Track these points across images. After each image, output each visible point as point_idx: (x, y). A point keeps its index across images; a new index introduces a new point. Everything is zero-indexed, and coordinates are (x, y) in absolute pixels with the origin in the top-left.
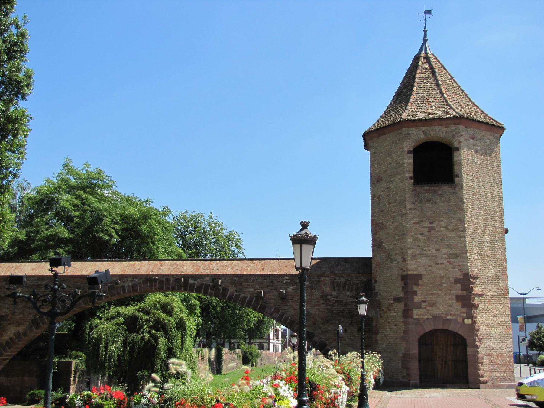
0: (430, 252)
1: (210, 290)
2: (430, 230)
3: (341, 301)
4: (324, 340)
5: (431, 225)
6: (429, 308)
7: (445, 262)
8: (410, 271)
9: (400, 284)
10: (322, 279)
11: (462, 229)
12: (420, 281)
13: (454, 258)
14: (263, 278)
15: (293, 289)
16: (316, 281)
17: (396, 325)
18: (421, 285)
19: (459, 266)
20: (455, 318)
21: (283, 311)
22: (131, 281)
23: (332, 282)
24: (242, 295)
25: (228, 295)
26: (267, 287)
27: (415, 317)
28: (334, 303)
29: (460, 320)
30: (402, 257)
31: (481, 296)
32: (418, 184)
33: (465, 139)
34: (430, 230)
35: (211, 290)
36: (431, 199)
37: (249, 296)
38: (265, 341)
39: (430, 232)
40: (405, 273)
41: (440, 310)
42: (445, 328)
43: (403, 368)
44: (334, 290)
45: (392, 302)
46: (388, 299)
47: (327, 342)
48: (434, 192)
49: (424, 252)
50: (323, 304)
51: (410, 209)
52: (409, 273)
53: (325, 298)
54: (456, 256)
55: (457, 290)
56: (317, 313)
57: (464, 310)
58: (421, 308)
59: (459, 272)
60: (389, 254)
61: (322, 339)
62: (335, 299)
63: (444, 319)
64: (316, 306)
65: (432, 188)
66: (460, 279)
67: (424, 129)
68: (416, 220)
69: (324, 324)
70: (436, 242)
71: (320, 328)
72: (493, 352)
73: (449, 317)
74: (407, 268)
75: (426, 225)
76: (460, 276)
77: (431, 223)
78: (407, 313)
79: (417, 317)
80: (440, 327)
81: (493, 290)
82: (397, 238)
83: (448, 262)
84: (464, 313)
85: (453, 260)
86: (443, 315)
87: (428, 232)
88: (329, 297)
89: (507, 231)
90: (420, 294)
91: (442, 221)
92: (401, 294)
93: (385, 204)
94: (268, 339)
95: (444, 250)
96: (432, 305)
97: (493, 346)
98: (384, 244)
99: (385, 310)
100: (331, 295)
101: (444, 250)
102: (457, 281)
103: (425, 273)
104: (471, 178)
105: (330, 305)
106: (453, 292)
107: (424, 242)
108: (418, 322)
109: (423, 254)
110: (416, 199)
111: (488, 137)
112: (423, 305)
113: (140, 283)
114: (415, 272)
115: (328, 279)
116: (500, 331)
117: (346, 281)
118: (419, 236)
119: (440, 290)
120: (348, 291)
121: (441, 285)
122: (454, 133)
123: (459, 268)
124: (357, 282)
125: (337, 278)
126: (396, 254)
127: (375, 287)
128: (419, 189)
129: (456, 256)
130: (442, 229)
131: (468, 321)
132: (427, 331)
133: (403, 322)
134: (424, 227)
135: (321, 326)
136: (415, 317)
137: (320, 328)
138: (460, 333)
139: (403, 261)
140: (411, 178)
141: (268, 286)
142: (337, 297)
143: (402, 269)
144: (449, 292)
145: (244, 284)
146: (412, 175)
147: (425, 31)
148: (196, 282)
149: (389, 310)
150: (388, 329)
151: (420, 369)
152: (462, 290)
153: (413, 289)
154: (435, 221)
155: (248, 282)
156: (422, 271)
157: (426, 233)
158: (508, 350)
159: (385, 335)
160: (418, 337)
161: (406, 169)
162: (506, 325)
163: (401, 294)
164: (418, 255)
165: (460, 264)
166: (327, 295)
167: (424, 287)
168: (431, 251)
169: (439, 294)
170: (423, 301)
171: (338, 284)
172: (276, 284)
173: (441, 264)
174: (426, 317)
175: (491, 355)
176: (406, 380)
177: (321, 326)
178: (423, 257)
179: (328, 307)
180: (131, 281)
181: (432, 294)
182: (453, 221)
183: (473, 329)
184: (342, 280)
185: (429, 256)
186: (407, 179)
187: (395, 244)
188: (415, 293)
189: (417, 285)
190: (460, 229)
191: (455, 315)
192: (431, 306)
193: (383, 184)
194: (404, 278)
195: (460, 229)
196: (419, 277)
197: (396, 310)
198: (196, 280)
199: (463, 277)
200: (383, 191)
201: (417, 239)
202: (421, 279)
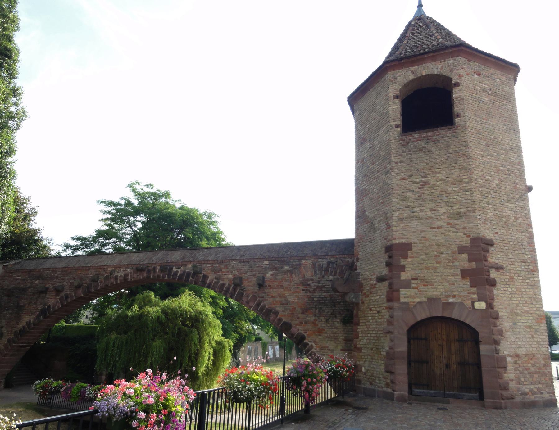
0: (423, 213)
1: (191, 278)
2: (423, 185)
3: (324, 287)
4: (302, 332)
5: (423, 179)
6: (422, 288)
8: (395, 239)
9: (384, 258)
10: (303, 262)
11: (467, 180)
12: (409, 251)
13: (457, 218)
14: (242, 263)
15: (272, 275)
16: (297, 265)
17: (378, 312)
18: (411, 257)
19: (464, 228)
20: (459, 300)
21: (261, 299)
22: (124, 271)
23: (314, 265)
24: (221, 282)
25: (208, 283)
26: (246, 273)
27: (402, 300)
28: (315, 289)
29: (468, 304)
30: (387, 224)
31: (499, 268)
32: (406, 132)
33: (468, 74)
34: (423, 185)
35: (192, 278)
36: (424, 147)
37: (227, 283)
39: (423, 188)
40: (389, 243)
41: (439, 290)
42: (446, 315)
43: (387, 372)
45: (375, 282)
46: (371, 279)
47: (305, 335)
48: (428, 138)
49: (415, 214)
50: (303, 290)
51: (396, 163)
52: (394, 242)
53: (305, 283)
54: (460, 215)
55: (463, 261)
56: (296, 301)
57: (474, 289)
58: (410, 288)
59: (464, 236)
60: (372, 223)
61: (300, 331)
62: (317, 284)
63: (443, 303)
64: (296, 292)
65: (425, 135)
66: (466, 247)
67: (413, 68)
68: (404, 175)
69: (303, 313)
70: (431, 200)
71: (298, 318)
72: (521, 352)
73: (451, 300)
74: (392, 236)
75: (417, 180)
76: (467, 242)
77: (422, 177)
78: (392, 296)
79: (406, 300)
80: (438, 313)
81: (516, 263)
82: (381, 201)
83: (448, 224)
84: (474, 294)
85: (456, 221)
86: (441, 297)
87: (419, 188)
88: (309, 282)
89: (530, 189)
90: (410, 268)
91: (439, 173)
92: (385, 271)
93: (368, 167)
95: (442, 210)
96: (426, 283)
97: (520, 343)
98: (366, 213)
99: (367, 294)
102: (462, 250)
103: (416, 240)
104: (478, 119)
105: (310, 292)
107: (413, 202)
108: (406, 307)
109: (413, 217)
110: (405, 149)
111: (499, 77)
112: (414, 284)
113: (131, 273)
114: (403, 241)
115: (309, 262)
116: (530, 321)
117: (329, 263)
118: (407, 194)
119: (437, 263)
120: (331, 275)
121: (439, 256)
122: (452, 67)
123: (465, 230)
124: (342, 264)
125: (320, 260)
126: (380, 221)
127: (356, 266)
128: (407, 138)
129: (460, 215)
130: (439, 183)
131: (481, 305)
132: (419, 319)
133: (387, 308)
134: (414, 183)
135: (300, 315)
136: (402, 300)
137: (298, 318)
138: (467, 322)
139: (387, 229)
140: (397, 126)
141: (247, 272)
142: (319, 282)
143: (386, 239)
144: (451, 264)
145: (223, 270)
146: (399, 122)
148: (179, 270)
149: (371, 293)
150: (370, 318)
151: (409, 374)
152: (470, 261)
153: (400, 263)
154: (429, 174)
155: (227, 268)
156: (411, 238)
157: (417, 190)
158: (542, 349)
159: (366, 325)
160: (406, 329)
161: (392, 117)
162: (537, 312)
163: (385, 271)
164: (407, 218)
165: (466, 225)
166: (308, 280)
167: (415, 259)
168: (426, 212)
169: (435, 268)
170: (413, 279)
171: (321, 268)
173: (438, 228)
174: (418, 300)
175: (517, 356)
176: (390, 390)
177: (300, 315)
178: (413, 220)
179: (308, 294)
180: (124, 271)
181: (426, 269)
182: (453, 171)
183: (490, 314)
184: (325, 262)
185: (421, 219)
186: (391, 129)
187: (378, 210)
188: (403, 268)
189: (406, 257)
190: (464, 180)
191: (459, 297)
192: (425, 285)
193: (367, 145)
194: (389, 249)
195: (464, 180)
196: (408, 246)
197: (379, 292)
198: (179, 268)
199: (471, 242)
200: (366, 152)
201: (404, 199)
202: (411, 249)
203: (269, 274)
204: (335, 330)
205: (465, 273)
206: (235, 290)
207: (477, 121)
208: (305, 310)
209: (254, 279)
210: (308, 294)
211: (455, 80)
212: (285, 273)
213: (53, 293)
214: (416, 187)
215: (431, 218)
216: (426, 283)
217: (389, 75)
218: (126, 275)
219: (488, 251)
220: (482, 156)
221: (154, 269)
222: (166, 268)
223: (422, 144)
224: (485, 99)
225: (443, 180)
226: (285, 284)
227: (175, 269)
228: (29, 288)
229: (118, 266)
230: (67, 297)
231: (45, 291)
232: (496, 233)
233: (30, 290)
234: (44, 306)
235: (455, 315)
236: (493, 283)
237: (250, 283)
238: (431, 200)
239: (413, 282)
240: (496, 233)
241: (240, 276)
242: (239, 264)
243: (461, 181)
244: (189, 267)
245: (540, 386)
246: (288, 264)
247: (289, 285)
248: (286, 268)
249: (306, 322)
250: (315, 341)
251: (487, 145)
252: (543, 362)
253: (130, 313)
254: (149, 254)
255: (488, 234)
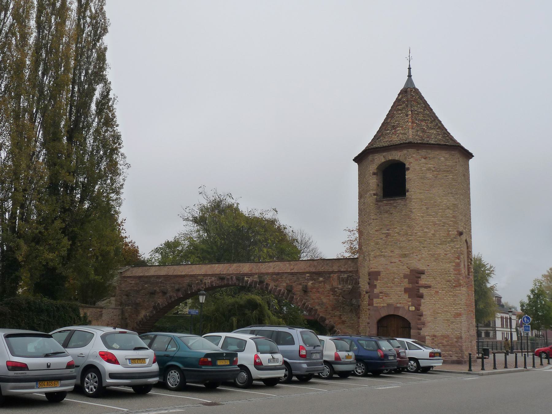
2: (388, 235)
6: (384, 298)
7: (397, 260)
10: (332, 275)
13: (404, 257)
16: (328, 277)
23: (339, 278)
24: (278, 289)
26: (294, 282)
29: (406, 307)
31: (427, 287)
38: (491, 329)
44: (340, 284)
51: (373, 219)
53: (333, 290)
54: (405, 256)
55: (406, 283)
67: (384, 154)
70: (391, 245)
71: (330, 314)
73: (398, 305)
76: (407, 272)
77: (388, 230)
79: (376, 305)
94: (494, 327)
95: (397, 252)
96: (387, 295)
100: (338, 288)
101: (397, 252)
103: (382, 270)
106: (402, 284)
114: (376, 270)
115: (336, 275)
125: (342, 274)
136: (374, 305)
137: (330, 314)
142: (342, 289)
147: (410, 69)
156: (380, 269)
160: (376, 321)
166: (335, 288)
171: (343, 280)
172: (301, 279)
173: (394, 263)
174: (382, 305)
175: (435, 336)
179: (336, 297)
189: (377, 280)
196: (378, 273)
203: (310, 283)
204: (352, 322)
205: (406, 290)
206: (288, 294)
207: (421, 193)
208: (334, 308)
209: (301, 287)
210: (336, 297)
211: (407, 166)
212: (320, 282)
213: (160, 294)
214: (383, 236)
215: (391, 256)
216: (387, 295)
217: (370, 157)
218: (212, 282)
219: (420, 277)
220: (422, 217)
221: (232, 278)
222: (240, 277)
223: (387, 208)
224: (429, 175)
225: (398, 233)
226: (321, 290)
227: (246, 279)
228: (141, 290)
229: (205, 275)
230: (171, 297)
231: (153, 293)
232: (428, 266)
233: (142, 292)
234: (155, 303)
235: (400, 313)
236: (421, 296)
237: (297, 289)
238: (391, 245)
239: (380, 294)
240: (428, 266)
241: (291, 284)
242: (290, 276)
243: (407, 234)
244: (256, 278)
245: (450, 352)
246: (322, 277)
247: (323, 291)
248: (321, 279)
249: (335, 316)
250: (340, 329)
251: (427, 209)
252: (455, 340)
253: (27, 59)
254: (227, 265)
255: (421, 266)
